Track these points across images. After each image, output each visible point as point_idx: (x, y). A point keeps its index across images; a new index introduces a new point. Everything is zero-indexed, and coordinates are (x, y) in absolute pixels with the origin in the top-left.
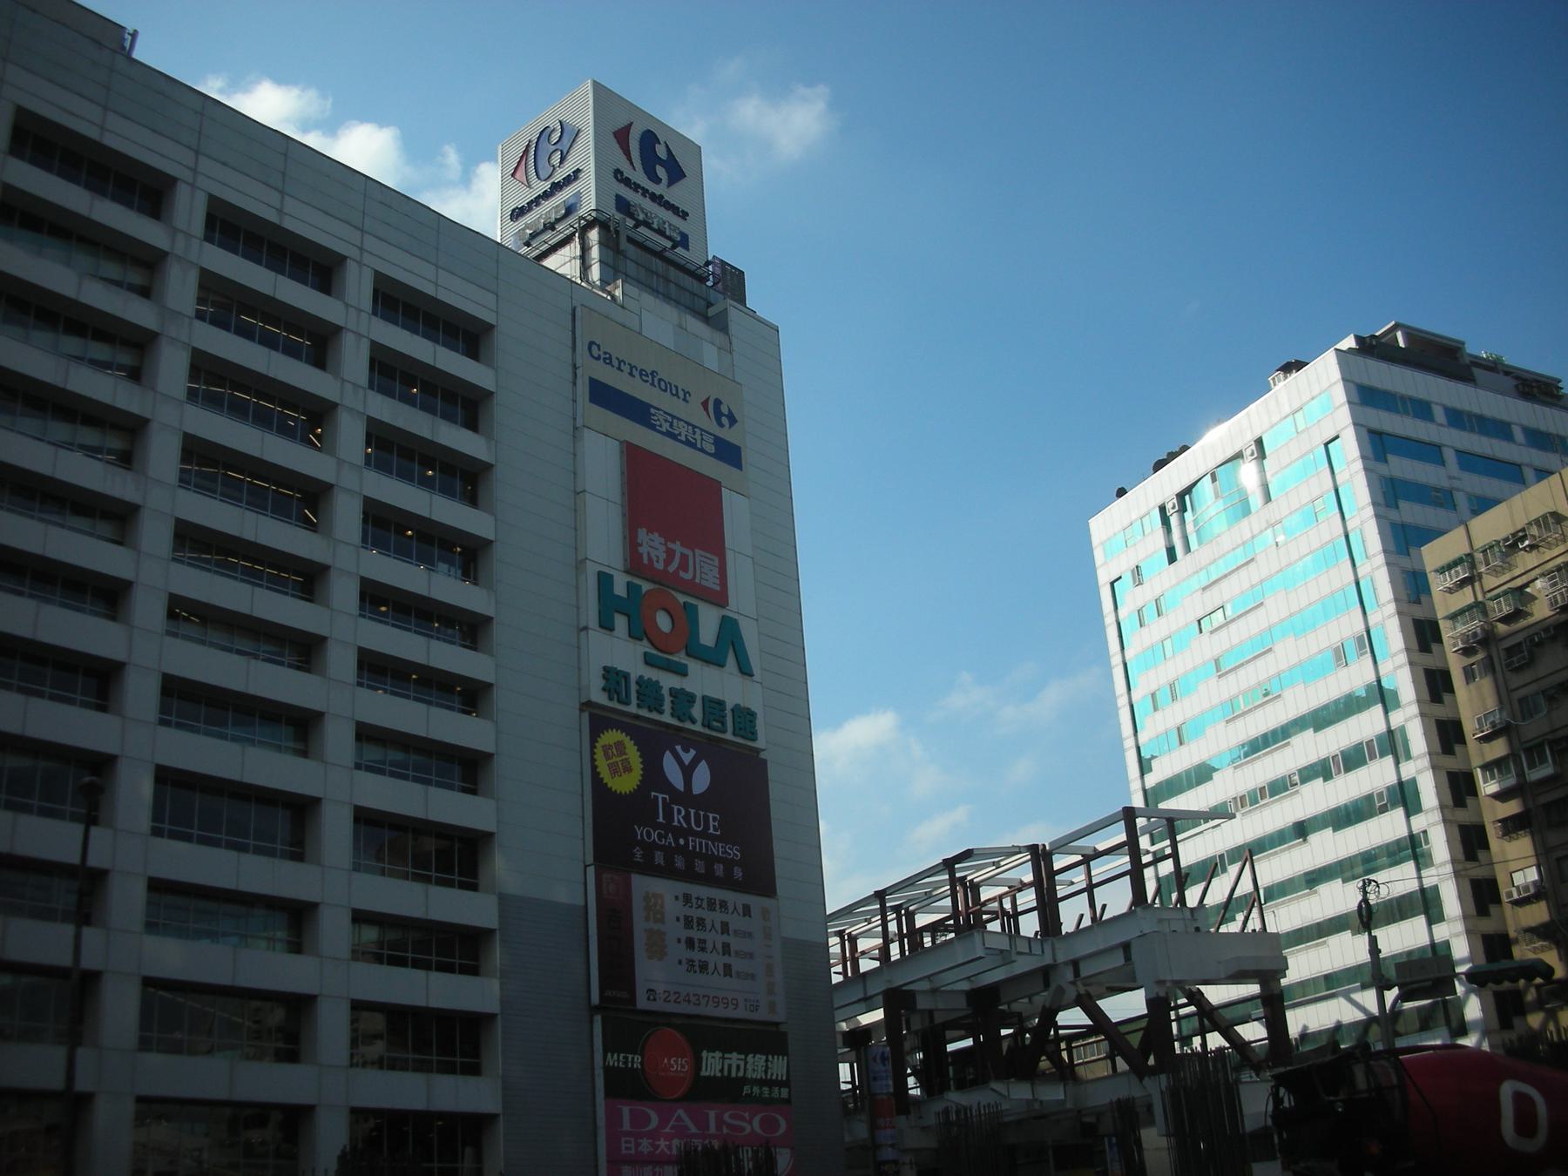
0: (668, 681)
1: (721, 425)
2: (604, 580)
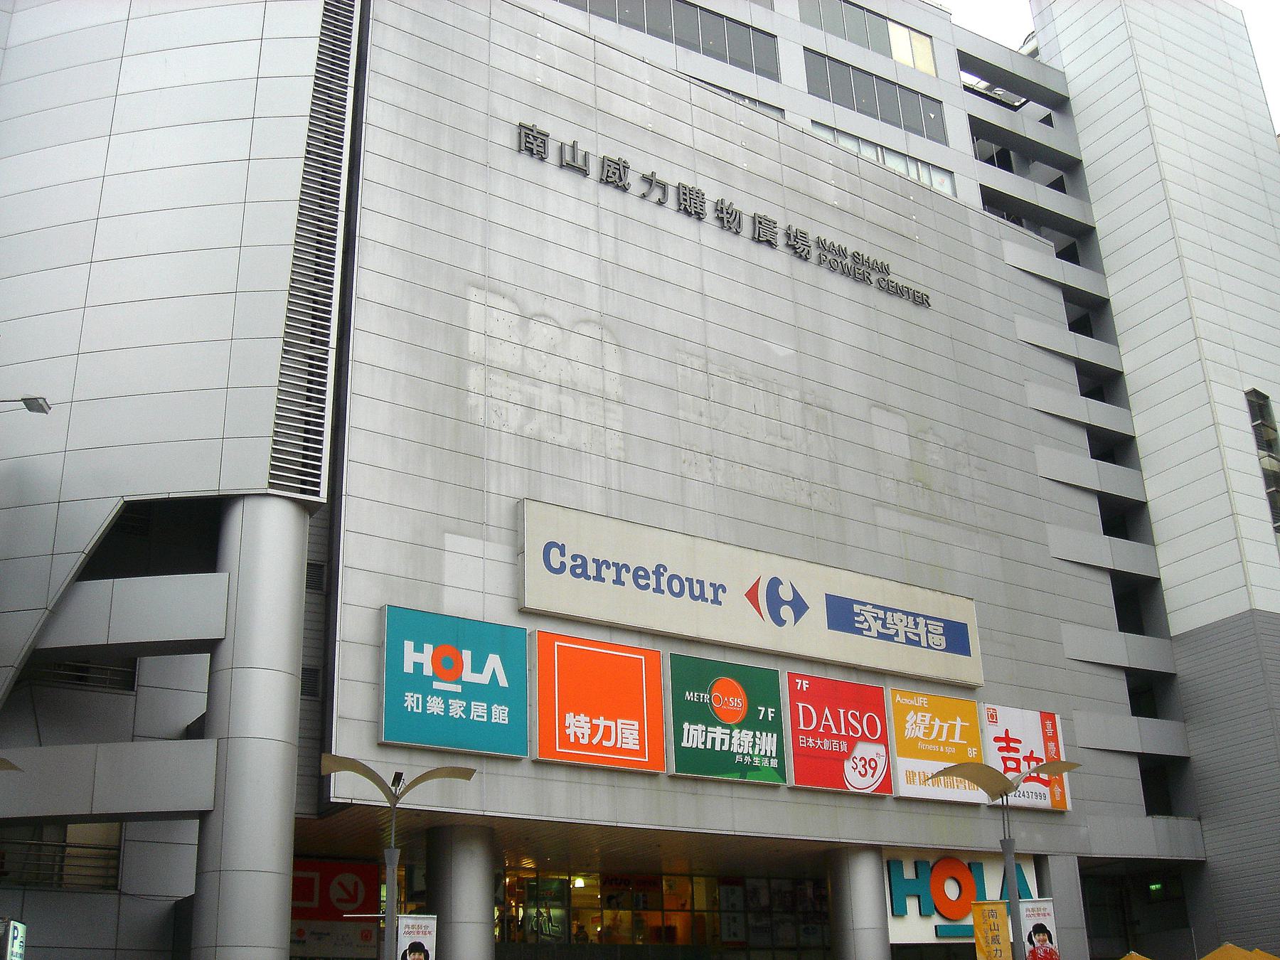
1: (780, 622)
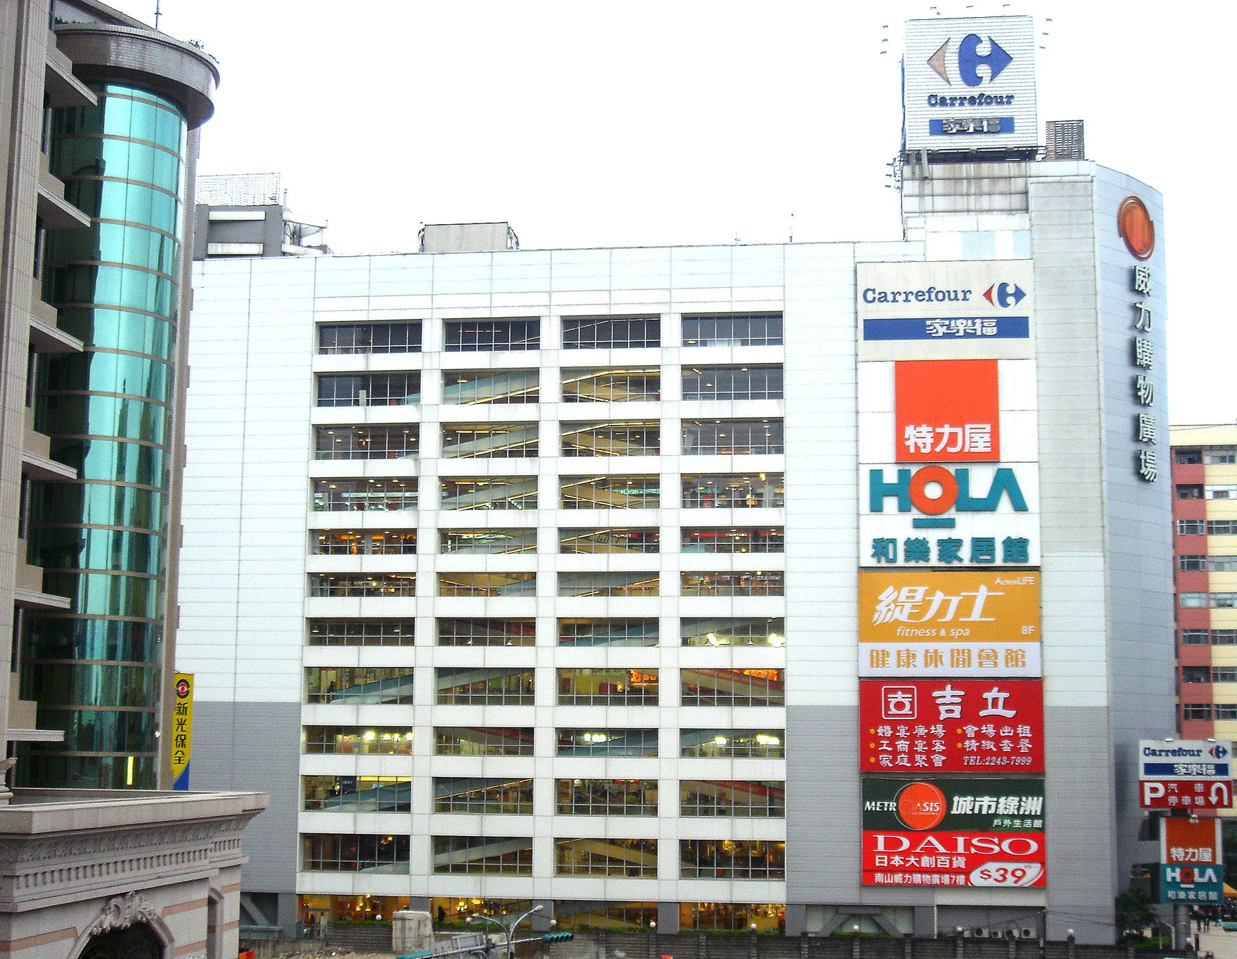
0: (933, 537)
2: (876, 475)
